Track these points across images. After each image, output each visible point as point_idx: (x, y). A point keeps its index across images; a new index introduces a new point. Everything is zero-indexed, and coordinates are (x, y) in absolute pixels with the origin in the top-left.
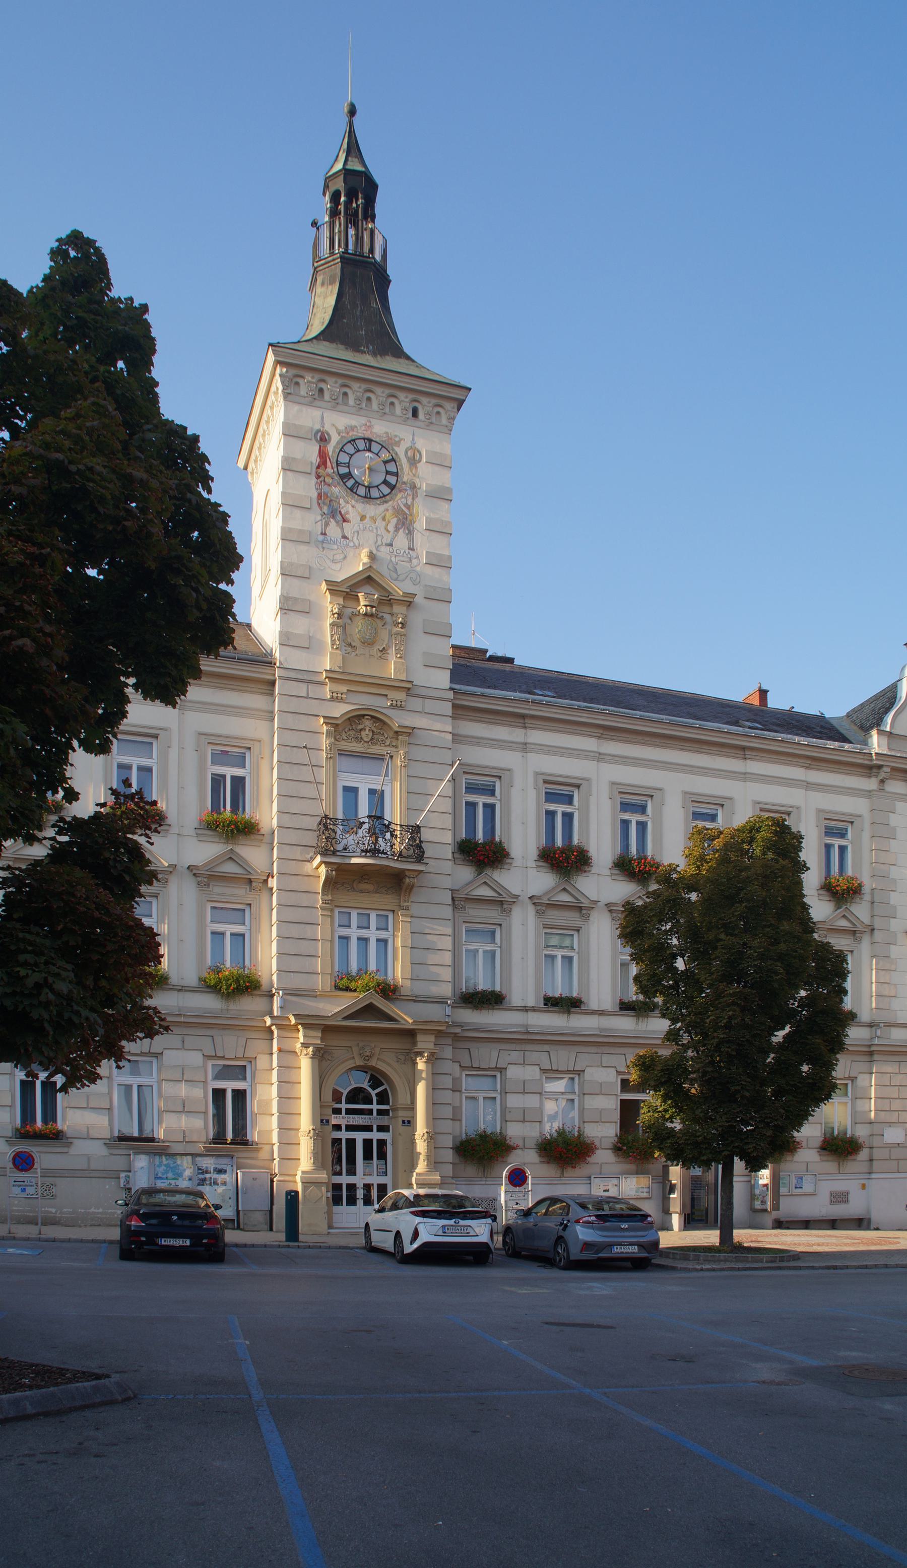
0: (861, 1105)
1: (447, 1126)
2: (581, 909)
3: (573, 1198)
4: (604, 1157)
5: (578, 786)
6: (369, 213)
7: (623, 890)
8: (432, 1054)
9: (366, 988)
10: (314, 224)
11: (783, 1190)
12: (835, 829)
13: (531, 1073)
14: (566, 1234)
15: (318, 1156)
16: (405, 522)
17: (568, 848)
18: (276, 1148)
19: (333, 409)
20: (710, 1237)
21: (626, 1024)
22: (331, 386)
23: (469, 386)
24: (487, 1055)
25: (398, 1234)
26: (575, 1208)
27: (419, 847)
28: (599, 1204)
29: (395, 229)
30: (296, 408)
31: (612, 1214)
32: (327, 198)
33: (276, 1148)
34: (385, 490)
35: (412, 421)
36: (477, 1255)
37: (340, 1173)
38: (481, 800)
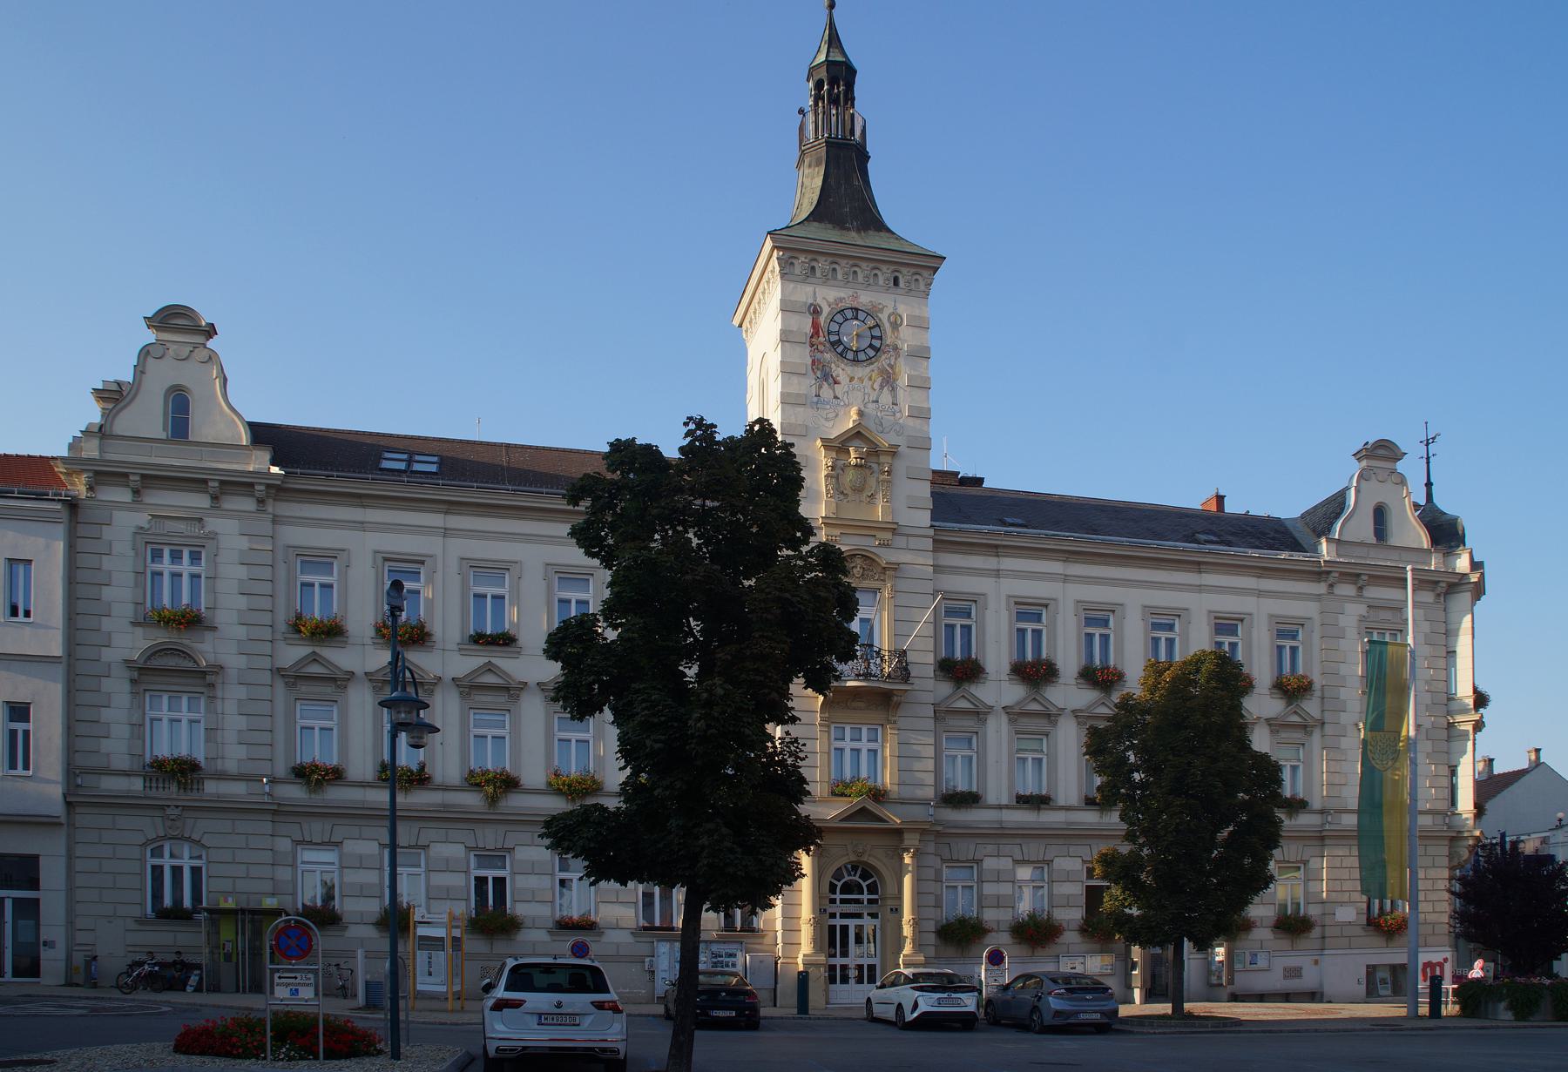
0: (1313, 886)
1: (930, 913)
2: (1050, 716)
3: (1046, 974)
4: (1071, 937)
5: (1046, 606)
6: (850, 98)
7: (1084, 697)
8: (917, 850)
9: (860, 794)
10: (801, 111)
11: (1238, 966)
12: (1286, 631)
13: (1006, 863)
14: (1040, 1005)
15: (816, 941)
16: (889, 380)
17: (1038, 662)
18: (779, 935)
19: (824, 284)
20: (1165, 1008)
21: (1090, 817)
22: (822, 265)
23: (940, 253)
24: (965, 849)
25: (900, 1006)
26: (1047, 982)
27: (906, 669)
28: (1067, 979)
29: (871, 106)
30: (792, 285)
31: (1078, 987)
32: (811, 84)
33: (779, 935)
34: (871, 353)
35: (894, 290)
36: (965, 1022)
37: (834, 956)
38: (958, 622)
